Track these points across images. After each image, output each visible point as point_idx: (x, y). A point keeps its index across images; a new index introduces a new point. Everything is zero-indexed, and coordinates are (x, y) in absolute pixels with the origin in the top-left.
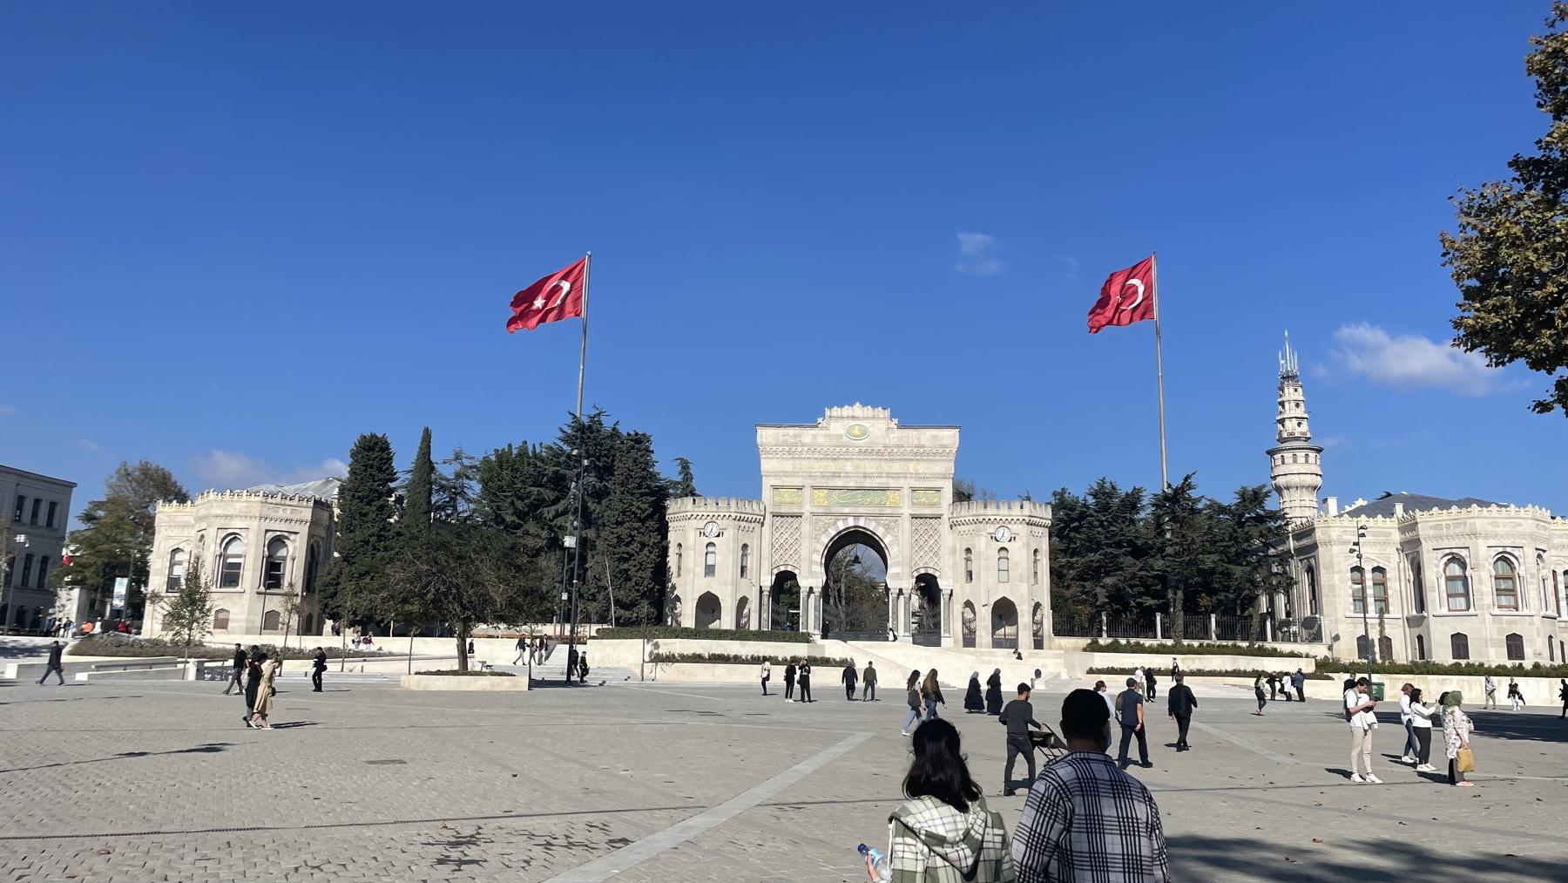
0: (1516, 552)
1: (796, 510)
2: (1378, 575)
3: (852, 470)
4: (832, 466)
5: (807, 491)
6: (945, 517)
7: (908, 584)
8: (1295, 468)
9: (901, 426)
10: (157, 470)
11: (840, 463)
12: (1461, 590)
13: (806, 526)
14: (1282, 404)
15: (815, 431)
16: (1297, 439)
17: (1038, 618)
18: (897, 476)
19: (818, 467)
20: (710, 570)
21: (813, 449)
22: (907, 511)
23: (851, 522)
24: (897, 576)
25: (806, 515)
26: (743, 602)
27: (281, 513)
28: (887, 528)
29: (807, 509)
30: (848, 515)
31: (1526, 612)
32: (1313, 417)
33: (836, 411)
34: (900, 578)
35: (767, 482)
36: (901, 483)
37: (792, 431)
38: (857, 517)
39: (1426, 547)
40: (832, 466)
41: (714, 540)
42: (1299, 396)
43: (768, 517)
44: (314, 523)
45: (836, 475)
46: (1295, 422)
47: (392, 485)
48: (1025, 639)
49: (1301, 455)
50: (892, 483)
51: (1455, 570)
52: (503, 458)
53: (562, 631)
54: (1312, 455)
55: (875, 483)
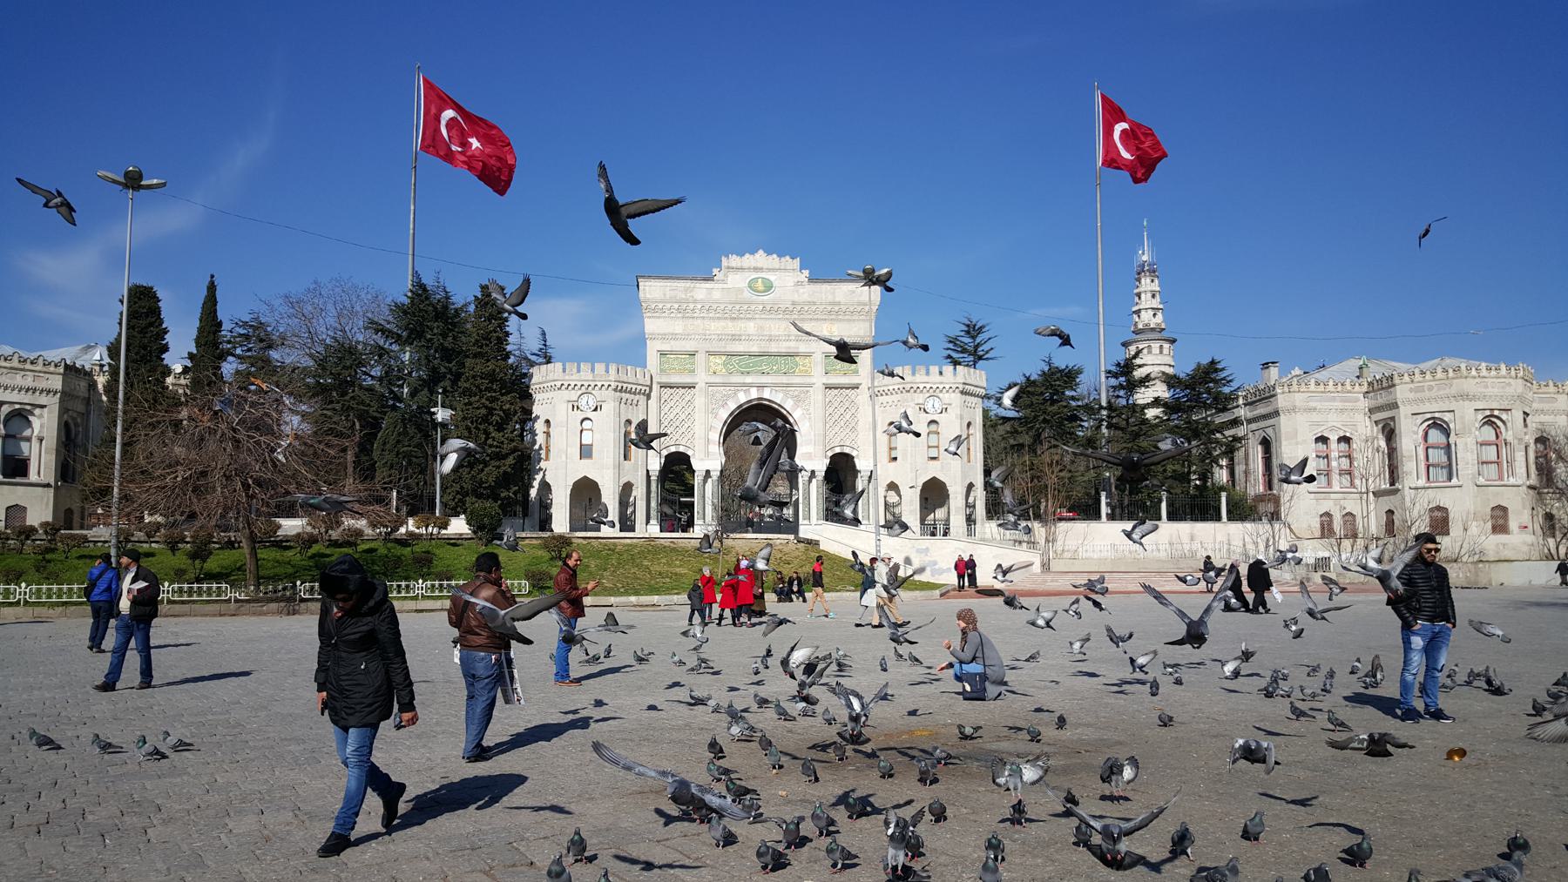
0: (1504, 417)
1: (687, 380)
2: (1343, 446)
3: (755, 333)
4: (731, 327)
5: (700, 357)
6: (864, 387)
7: (821, 466)
9: (812, 280)
11: (741, 324)
12: (1494, 458)
13: (699, 399)
14: (1139, 295)
15: (708, 285)
16: (1153, 330)
17: (971, 500)
19: (716, 327)
20: (586, 452)
21: (709, 309)
23: (754, 394)
24: (809, 456)
25: (701, 385)
26: (627, 488)
27: (18, 380)
28: (798, 401)
29: (701, 378)
30: (750, 385)
31: (1512, 481)
32: (1166, 308)
33: (734, 261)
34: (812, 457)
35: (653, 348)
37: (681, 284)
38: (761, 387)
39: (1404, 412)
40: (731, 327)
42: (1156, 287)
43: (655, 386)
44: (66, 396)
45: (735, 338)
46: (1151, 313)
48: (958, 522)
49: (1155, 346)
51: (1436, 436)
54: (1166, 346)
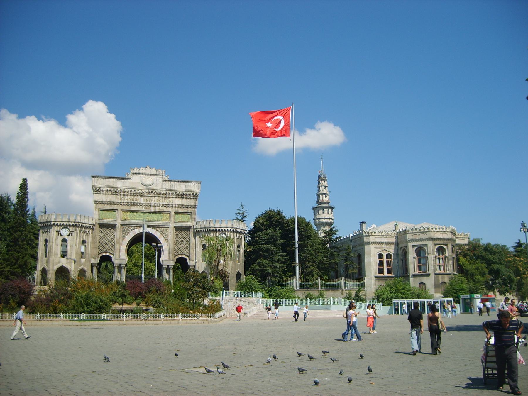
5: (119, 212)
8: (323, 216)
10: (495, 245)
13: (118, 232)
16: (325, 203)
18: (167, 206)
22: (172, 225)
25: (118, 225)
29: (119, 222)
36: (170, 209)
40: (163, 201)
41: (66, 238)
47: (167, 258)
49: (326, 210)
50: (165, 209)
53: (495, 374)
55: (157, 209)
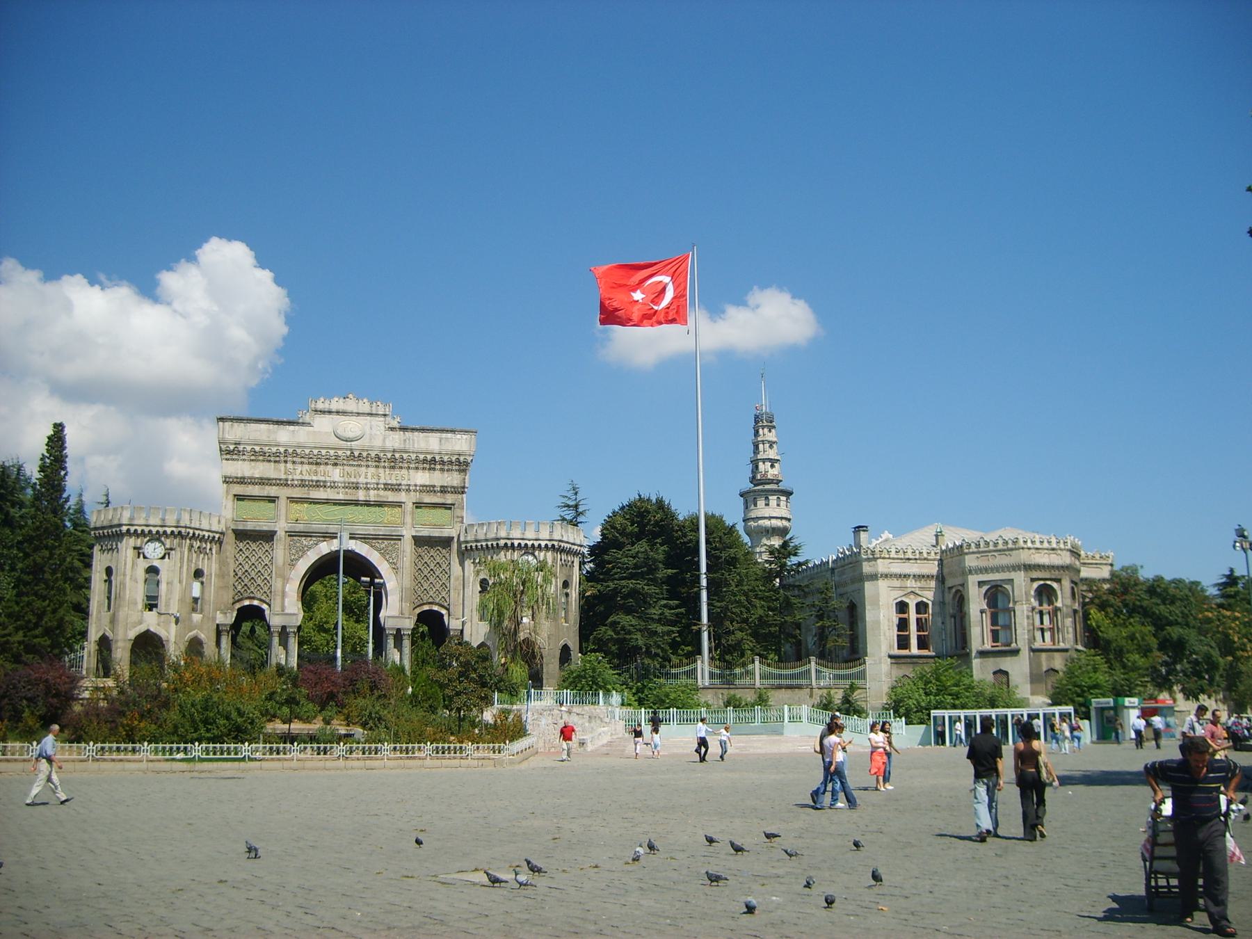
5: (283, 502)
8: (767, 512)
13: (280, 551)
16: (771, 482)
18: (395, 488)
22: (408, 533)
25: (281, 534)
29: (281, 527)
36: (402, 497)
40: (386, 476)
41: (156, 563)
49: (773, 499)
50: (391, 497)
52: (1124, 583)
55: (373, 496)
